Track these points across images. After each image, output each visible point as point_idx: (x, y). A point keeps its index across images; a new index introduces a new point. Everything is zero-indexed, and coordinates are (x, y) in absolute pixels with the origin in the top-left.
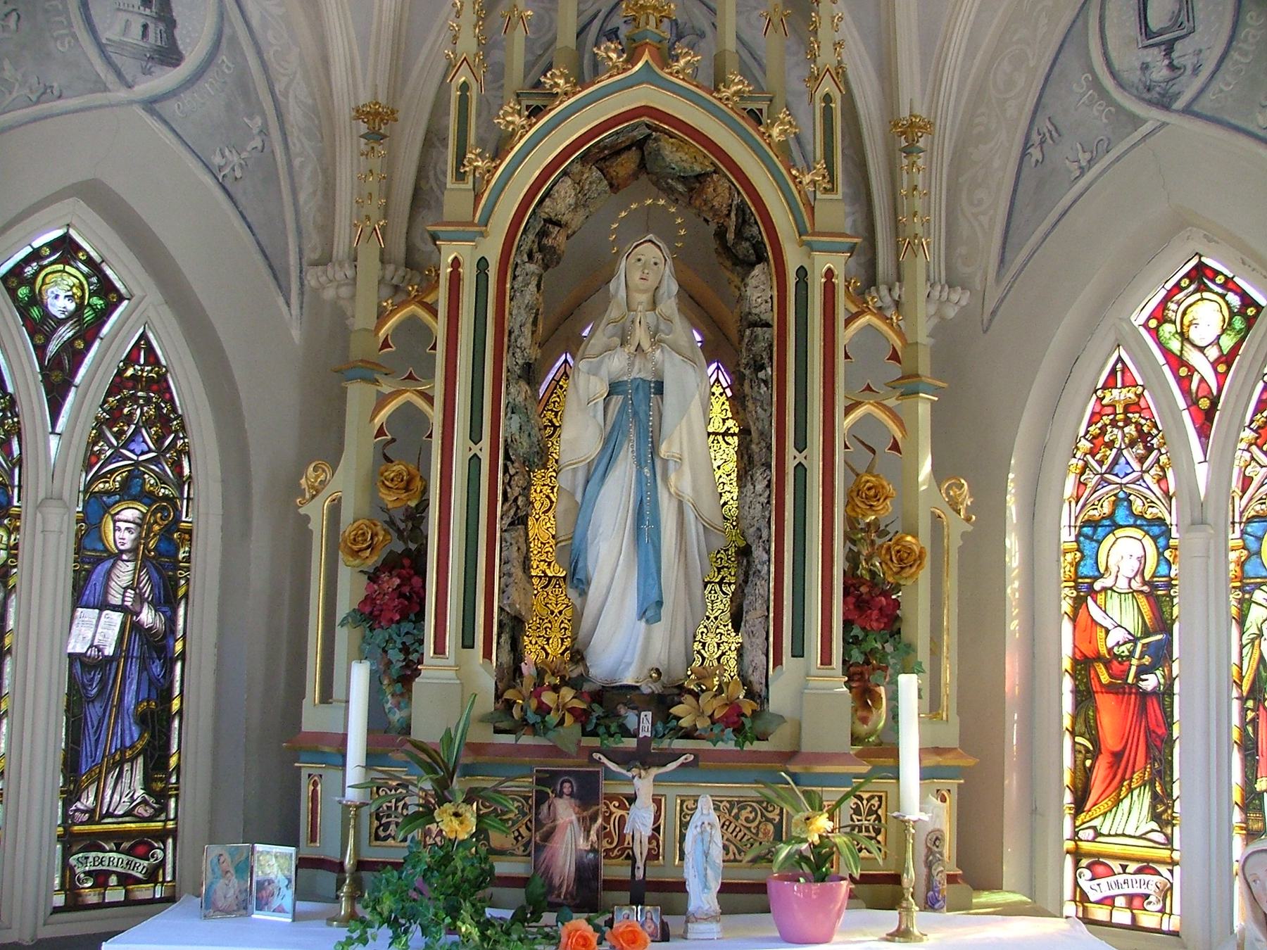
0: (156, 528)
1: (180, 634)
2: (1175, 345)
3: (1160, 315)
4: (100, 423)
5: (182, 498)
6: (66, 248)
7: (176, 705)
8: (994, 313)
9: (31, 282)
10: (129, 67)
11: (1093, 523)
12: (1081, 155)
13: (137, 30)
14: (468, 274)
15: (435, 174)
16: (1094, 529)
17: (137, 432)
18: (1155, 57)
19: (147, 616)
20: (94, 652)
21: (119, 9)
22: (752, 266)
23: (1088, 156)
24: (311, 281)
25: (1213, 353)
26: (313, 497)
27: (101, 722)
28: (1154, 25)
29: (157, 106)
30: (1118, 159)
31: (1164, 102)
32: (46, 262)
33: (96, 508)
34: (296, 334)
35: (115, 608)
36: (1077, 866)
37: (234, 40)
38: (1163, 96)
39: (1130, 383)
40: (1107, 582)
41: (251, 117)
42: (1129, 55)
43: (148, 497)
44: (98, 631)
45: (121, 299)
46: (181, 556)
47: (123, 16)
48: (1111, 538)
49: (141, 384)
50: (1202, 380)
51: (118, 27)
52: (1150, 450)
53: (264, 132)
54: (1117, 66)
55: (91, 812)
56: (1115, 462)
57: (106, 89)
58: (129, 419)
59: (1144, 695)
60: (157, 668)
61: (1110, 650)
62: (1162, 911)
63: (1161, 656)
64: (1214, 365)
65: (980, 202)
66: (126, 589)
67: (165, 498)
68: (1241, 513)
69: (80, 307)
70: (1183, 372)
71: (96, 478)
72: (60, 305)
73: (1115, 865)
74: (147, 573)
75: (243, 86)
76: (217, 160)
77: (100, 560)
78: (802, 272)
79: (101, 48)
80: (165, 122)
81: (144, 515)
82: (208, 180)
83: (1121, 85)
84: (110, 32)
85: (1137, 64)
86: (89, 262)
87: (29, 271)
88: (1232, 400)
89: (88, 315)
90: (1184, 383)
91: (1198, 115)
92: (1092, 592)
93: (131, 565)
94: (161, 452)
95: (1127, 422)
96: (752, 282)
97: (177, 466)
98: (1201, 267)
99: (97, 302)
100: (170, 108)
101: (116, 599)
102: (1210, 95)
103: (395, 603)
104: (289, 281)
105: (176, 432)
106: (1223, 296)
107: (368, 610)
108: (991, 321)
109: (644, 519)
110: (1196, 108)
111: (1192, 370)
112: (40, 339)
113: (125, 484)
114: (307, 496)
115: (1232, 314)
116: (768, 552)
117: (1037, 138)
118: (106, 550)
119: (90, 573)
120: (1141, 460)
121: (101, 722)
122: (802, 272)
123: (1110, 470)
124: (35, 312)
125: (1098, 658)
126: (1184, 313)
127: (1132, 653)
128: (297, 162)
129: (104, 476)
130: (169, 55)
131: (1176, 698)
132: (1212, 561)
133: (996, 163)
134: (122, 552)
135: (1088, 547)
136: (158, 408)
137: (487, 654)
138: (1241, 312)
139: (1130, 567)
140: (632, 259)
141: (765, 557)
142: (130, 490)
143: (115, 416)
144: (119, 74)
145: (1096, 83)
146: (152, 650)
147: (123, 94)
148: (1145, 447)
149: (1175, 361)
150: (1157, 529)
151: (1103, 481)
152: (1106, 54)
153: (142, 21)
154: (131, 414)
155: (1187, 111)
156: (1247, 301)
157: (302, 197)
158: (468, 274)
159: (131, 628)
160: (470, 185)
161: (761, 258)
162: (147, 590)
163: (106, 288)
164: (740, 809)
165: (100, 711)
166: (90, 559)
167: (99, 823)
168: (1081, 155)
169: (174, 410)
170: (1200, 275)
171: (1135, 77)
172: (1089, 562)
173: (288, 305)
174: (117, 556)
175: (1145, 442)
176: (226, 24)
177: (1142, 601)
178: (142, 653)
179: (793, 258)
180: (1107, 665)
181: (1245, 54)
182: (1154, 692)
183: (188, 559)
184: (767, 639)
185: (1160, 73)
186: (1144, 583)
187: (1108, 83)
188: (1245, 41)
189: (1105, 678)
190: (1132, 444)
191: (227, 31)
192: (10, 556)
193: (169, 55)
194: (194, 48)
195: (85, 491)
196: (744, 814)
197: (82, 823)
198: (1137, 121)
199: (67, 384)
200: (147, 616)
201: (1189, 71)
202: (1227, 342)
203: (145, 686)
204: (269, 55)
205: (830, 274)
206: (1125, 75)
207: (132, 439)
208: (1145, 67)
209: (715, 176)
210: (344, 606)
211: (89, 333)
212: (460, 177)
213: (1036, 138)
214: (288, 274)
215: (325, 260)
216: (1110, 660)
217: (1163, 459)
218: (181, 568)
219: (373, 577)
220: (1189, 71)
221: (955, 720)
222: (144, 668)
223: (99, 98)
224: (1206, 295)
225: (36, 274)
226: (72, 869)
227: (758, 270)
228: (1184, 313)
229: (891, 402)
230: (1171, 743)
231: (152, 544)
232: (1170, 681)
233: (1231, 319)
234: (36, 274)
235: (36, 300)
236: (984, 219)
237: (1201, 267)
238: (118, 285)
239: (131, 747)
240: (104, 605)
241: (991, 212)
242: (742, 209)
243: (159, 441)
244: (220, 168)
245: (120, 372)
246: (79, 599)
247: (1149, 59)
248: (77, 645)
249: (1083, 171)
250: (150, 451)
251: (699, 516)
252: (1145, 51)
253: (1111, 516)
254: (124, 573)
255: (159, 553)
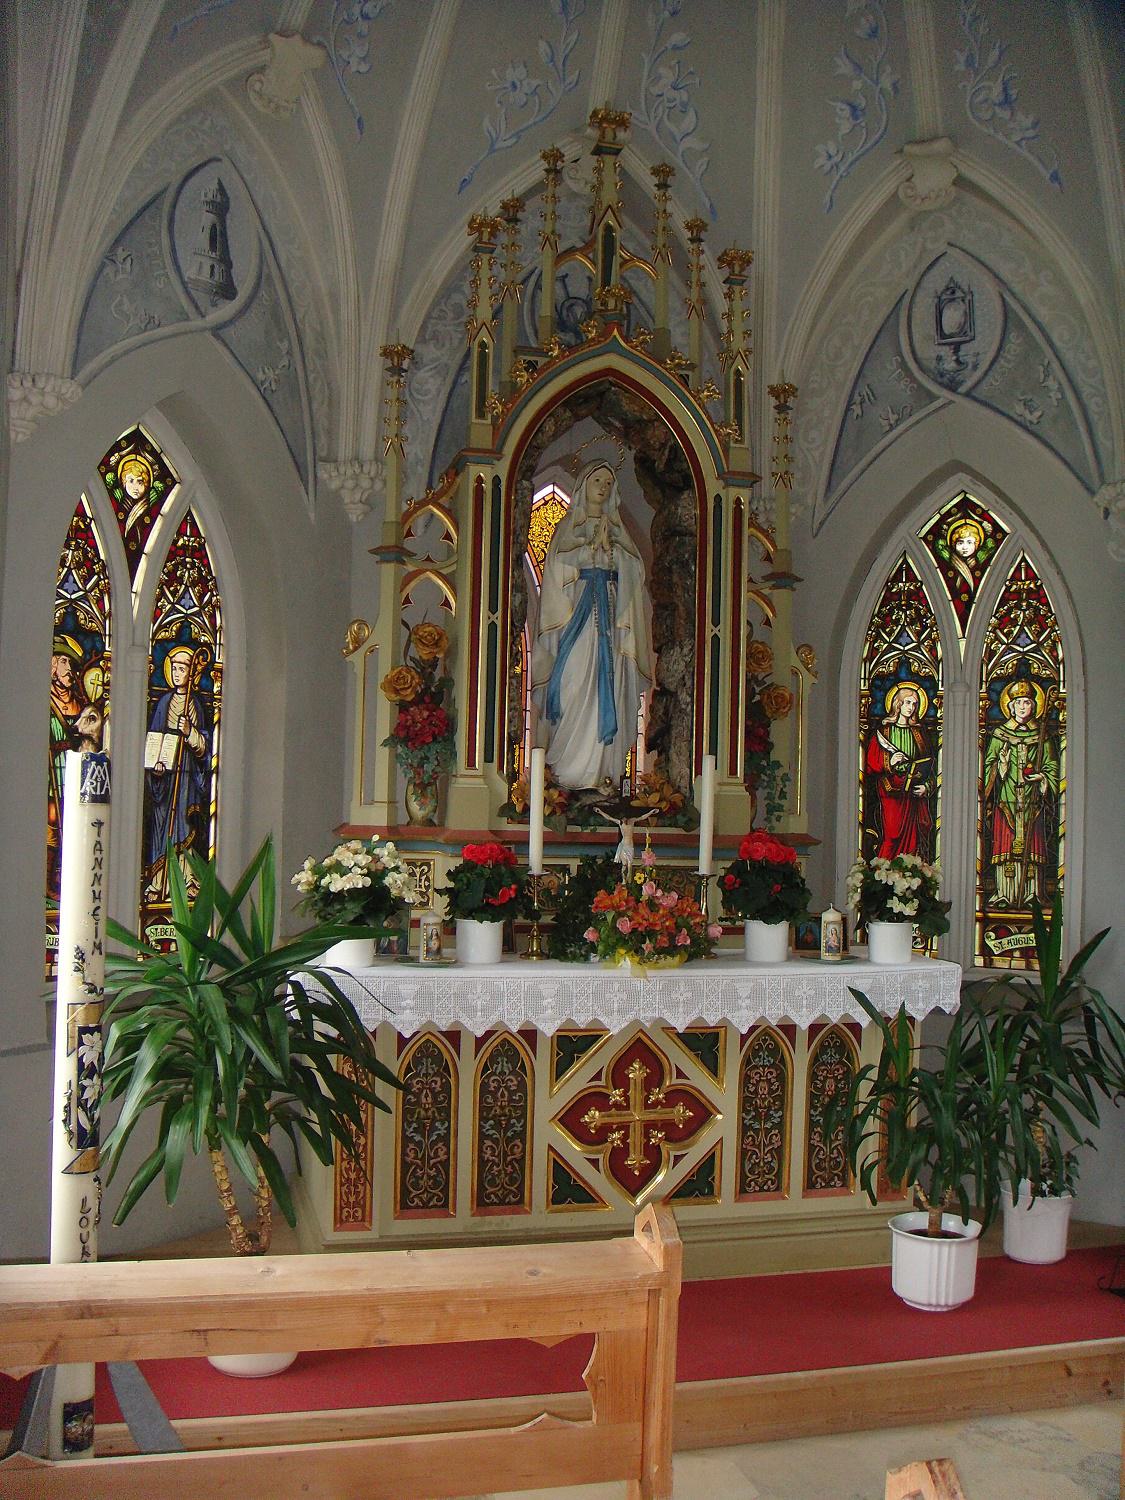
0: (199, 668)
1: (215, 752)
2: (946, 554)
3: (937, 532)
4: (162, 584)
5: (216, 644)
6: (137, 442)
7: (212, 809)
8: (822, 524)
9: (114, 470)
10: (203, 299)
11: (881, 677)
12: (890, 415)
13: (207, 270)
14: (487, 486)
15: (411, 394)
16: (881, 684)
17: (186, 591)
18: (946, 352)
19: (195, 739)
20: (159, 768)
21: (195, 253)
22: (680, 490)
23: (896, 416)
24: (323, 475)
25: (972, 562)
26: (356, 649)
27: (165, 822)
28: (947, 330)
29: (220, 332)
30: (918, 422)
31: (952, 386)
32: (124, 452)
33: (162, 649)
34: (312, 516)
35: (173, 732)
36: (983, 932)
37: (269, 276)
38: (951, 382)
39: (911, 578)
40: (893, 719)
41: (281, 341)
42: (929, 351)
43: (193, 643)
44: (160, 751)
45: (174, 482)
46: (216, 690)
47: (200, 259)
48: (896, 689)
49: (187, 553)
50: (964, 581)
51: (194, 269)
52: (924, 628)
53: (289, 353)
54: (919, 354)
55: (159, 893)
56: (900, 634)
57: (187, 319)
58: (180, 581)
59: (917, 799)
60: (200, 779)
61: (893, 767)
62: (925, 948)
63: (929, 773)
64: (972, 571)
65: (814, 440)
66: (180, 716)
67: (206, 644)
68: (988, 675)
69: (148, 489)
70: (951, 574)
71: (160, 628)
72: (134, 489)
73: (1013, 929)
74: (195, 703)
75: (276, 317)
76: (260, 376)
77: (166, 692)
78: (718, 498)
79: (184, 283)
80: (226, 345)
81: (192, 657)
82: (254, 392)
83: (921, 368)
84: (190, 273)
85: (934, 355)
86: (153, 452)
87: (113, 460)
88: (986, 595)
89: (153, 496)
90: (950, 583)
91: (975, 399)
92: (882, 728)
93: (183, 697)
94: (202, 608)
95: (909, 607)
96: (683, 503)
97: (212, 617)
98: (965, 501)
99: (158, 484)
100: (229, 333)
101: (173, 725)
102: (984, 386)
103: (424, 725)
104: (307, 472)
105: (211, 591)
106: (980, 523)
107: (403, 734)
108: (819, 529)
109: (604, 673)
110: (974, 394)
111: (957, 573)
112: (121, 516)
113: (179, 631)
114: (351, 647)
115: (986, 537)
116: (692, 696)
117: (860, 397)
118: (167, 686)
119: (156, 703)
120: (918, 634)
121: (165, 822)
122: (718, 498)
123: (896, 641)
124: (118, 494)
125: (884, 771)
126: (953, 532)
127: (908, 770)
128: (311, 379)
129: (165, 626)
130: (227, 291)
131: (939, 802)
132: (968, 707)
133: (826, 413)
134: (177, 687)
135: (879, 695)
136: (85, 553)
137: (501, 767)
138: (993, 536)
139: (906, 710)
140: (592, 479)
141: (689, 700)
142: (184, 638)
143: (172, 579)
144: (197, 307)
145: (903, 364)
146: (195, 763)
147: (198, 323)
148: (922, 626)
149: (946, 566)
150: (929, 684)
151: (891, 648)
152: (913, 352)
153: (210, 262)
154: (182, 576)
155: (968, 395)
156: (996, 527)
157: (315, 406)
158: (487, 486)
159: (184, 748)
160: (489, 421)
161: (690, 486)
162: (194, 717)
163: (164, 475)
164: (673, 875)
165: (164, 814)
166: (158, 690)
167: (164, 902)
168: (890, 415)
169: (210, 573)
170: (966, 508)
171: (932, 365)
172: (879, 706)
173: (306, 489)
174: (174, 691)
175: (921, 622)
176: (265, 267)
177: (918, 735)
178: (191, 769)
179: (713, 487)
180: (891, 779)
181: (1009, 361)
182: (923, 797)
183: (220, 693)
184: (690, 756)
185: (950, 365)
186: (918, 720)
187: (918, 374)
188: (1009, 352)
189: (888, 787)
190: (911, 624)
191: (265, 271)
192: (105, 691)
193: (227, 291)
194: (244, 277)
195: (153, 640)
196: (676, 879)
197: (154, 902)
198: (932, 397)
199: (140, 552)
200: (195, 739)
201: (970, 367)
202: (982, 556)
203: (193, 790)
204: (292, 291)
205: (738, 502)
206: (925, 362)
207: (182, 597)
208: (939, 359)
209: (656, 424)
210: (384, 730)
211: (153, 511)
212: (481, 414)
213: (857, 399)
214: (306, 467)
215: (332, 459)
216: (896, 775)
217: (934, 635)
218: (216, 700)
219: (403, 707)
220: (970, 367)
221: (805, 815)
222: (192, 780)
223: (183, 326)
224: (968, 521)
225: (118, 463)
226: (147, 937)
227: (686, 492)
228: (953, 532)
229: (766, 592)
230: (934, 833)
231: (196, 682)
232: (934, 789)
233: (985, 539)
234: (118, 463)
235: (118, 483)
236: (817, 454)
237: (965, 501)
238: (172, 470)
239: (185, 841)
240: (166, 730)
241: (822, 448)
242: (675, 449)
243: (201, 598)
244: (262, 383)
245: (175, 542)
246: (149, 729)
247: (942, 353)
248: (150, 763)
249: (892, 428)
250: (195, 606)
251: (639, 668)
252: (940, 348)
253: (896, 673)
254: (179, 703)
255: (202, 688)
